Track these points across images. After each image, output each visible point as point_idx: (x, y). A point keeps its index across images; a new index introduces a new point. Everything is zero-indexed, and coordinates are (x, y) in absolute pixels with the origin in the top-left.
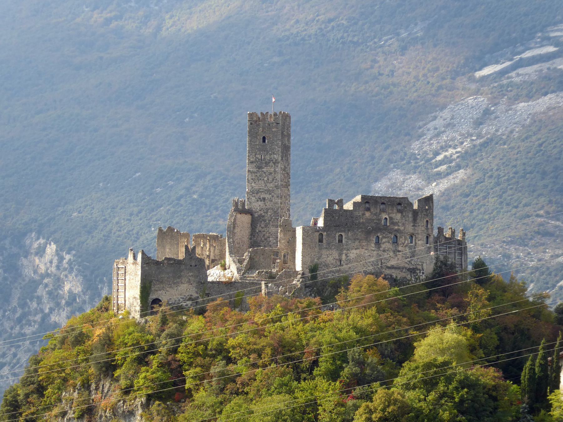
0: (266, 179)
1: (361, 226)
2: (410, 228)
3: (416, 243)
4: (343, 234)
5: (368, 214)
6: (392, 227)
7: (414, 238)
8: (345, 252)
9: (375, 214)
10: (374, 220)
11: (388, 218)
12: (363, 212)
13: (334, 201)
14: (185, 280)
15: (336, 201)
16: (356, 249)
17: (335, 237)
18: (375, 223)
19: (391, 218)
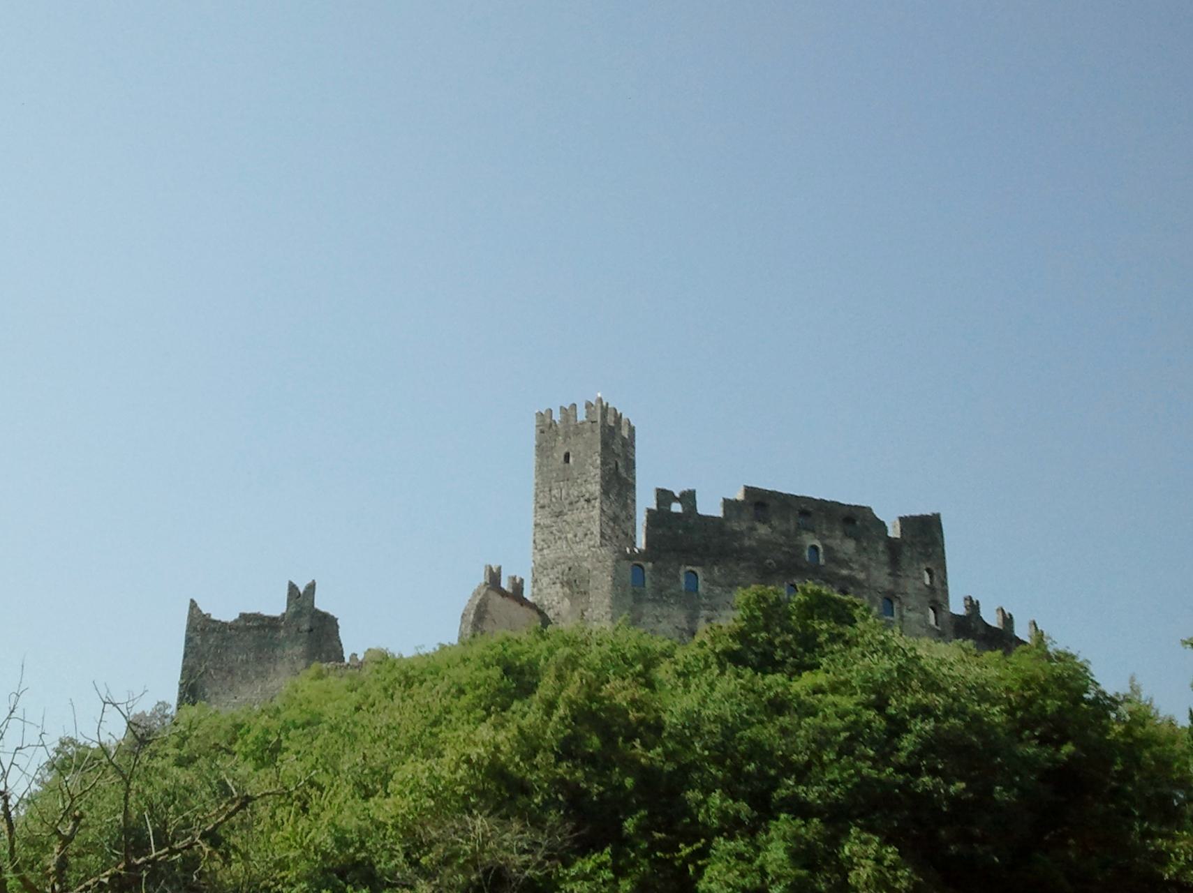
0: (570, 536)
2: (882, 577)
4: (698, 570)
5: (763, 530)
6: (832, 567)
7: (896, 605)
8: (704, 612)
11: (820, 546)
13: (672, 493)
17: (676, 578)
18: (784, 553)
19: (828, 549)
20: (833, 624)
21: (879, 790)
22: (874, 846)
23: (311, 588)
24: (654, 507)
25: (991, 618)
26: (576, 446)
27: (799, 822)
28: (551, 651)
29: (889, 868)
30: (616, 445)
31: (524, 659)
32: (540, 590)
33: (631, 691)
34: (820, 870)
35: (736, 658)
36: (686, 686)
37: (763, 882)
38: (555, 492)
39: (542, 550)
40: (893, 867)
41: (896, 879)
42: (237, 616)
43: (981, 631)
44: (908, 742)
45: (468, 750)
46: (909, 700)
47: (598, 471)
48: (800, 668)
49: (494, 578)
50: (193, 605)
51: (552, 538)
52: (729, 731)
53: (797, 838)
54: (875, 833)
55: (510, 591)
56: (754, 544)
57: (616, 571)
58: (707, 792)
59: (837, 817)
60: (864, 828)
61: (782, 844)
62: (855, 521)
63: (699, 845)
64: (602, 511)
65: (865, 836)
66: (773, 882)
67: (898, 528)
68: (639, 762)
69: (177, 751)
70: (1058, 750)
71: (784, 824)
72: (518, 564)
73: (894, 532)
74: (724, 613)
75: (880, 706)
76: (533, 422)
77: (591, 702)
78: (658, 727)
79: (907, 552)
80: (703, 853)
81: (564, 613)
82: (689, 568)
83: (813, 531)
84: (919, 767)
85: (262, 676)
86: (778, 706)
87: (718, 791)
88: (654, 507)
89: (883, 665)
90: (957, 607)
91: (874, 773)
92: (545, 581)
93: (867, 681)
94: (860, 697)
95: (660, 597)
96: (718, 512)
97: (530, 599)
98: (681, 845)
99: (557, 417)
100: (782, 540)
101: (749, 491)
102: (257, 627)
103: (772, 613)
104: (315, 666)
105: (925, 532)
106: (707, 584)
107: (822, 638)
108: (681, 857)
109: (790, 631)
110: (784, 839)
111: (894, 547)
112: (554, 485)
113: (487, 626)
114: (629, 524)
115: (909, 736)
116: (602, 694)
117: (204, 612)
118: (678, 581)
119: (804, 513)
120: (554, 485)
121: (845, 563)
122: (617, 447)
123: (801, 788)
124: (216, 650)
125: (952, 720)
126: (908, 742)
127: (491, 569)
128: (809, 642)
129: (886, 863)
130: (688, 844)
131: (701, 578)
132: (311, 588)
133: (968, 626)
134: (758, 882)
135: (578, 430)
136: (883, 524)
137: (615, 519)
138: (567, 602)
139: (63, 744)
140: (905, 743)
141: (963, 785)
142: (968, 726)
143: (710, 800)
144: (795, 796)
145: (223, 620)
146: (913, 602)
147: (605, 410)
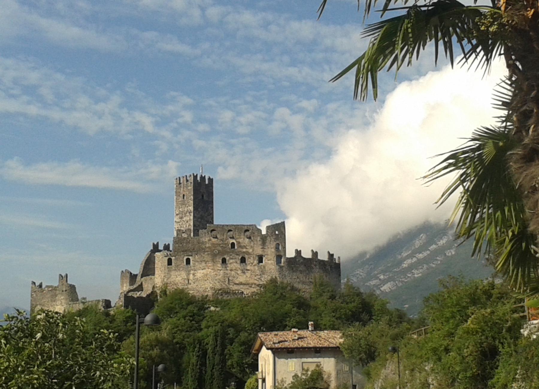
8: (192, 272)
12: (208, 238)
14: (58, 303)
17: (183, 261)
74: (199, 271)
118: (184, 262)
121: (245, 247)
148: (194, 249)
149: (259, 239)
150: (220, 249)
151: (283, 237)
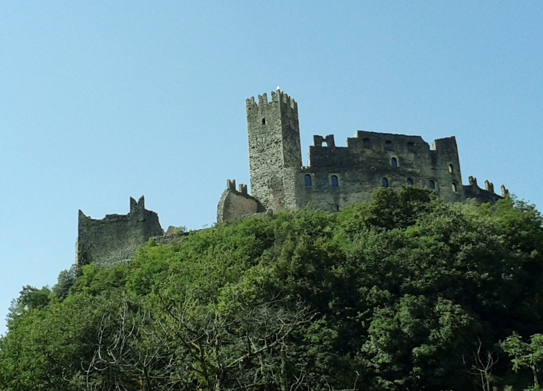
0: (268, 161)
1: (361, 165)
2: (428, 171)
3: (439, 189)
4: (337, 175)
5: (368, 152)
8: (342, 195)
9: (379, 153)
10: (377, 159)
12: (361, 150)
13: (322, 137)
14: (132, 240)
15: (324, 138)
16: (357, 192)
17: (327, 179)
19: (401, 159)
20: (419, 202)
21: (450, 280)
22: (450, 305)
23: (142, 199)
24: (313, 145)
25: (483, 186)
26: (269, 116)
27: (414, 297)
28: (279, 225)
29: (457, 314)
30: (288, 112)
31: (266, 229)
32: (255, 190)
33: (328, 243)
34: (426, 318)
35: (373, 222)
36: (351, 237)
37: (399, 326)
38: (259, 140)
39: (254, 170)
40: (459, 314)
41: (461, 320)
42: (105, 217)
43: (478, 193)
44: (460, 256)
45: (254, 278)
46: (459, 236)
47: (281, 127)
48: (405, 225)
49: (232, 186)
50: (80, 212)
51: (259, 163)
52: (378, 259)
53: (413, 304)
54: (449, 300)
55: (241, 191)
56: (364, 159)
57: (297, 179)
58: (370, 287)
59: (430, 293)
60: (444, 297)
61: (407, 308)
62: (414, 143)
63: (367, 312)
64: (284, 147)
65: (445, 301)
66: (403, 326)
67: (435, 145)
68: (334, 276)
69: (87, 288)
70: (530, 254)
71: (407, 299)
72: (243, 178)
73: (433, 148)
74: (352, 195)
75: (446, 240)
76: (245, 104)
77: (310, 250)
78: (344, 258)
79: (440, 158)
80: (370, 315)
81: (270, 201)
82: (333, 174)
83: (393, 151)
84: (466, 267)
85: (120, 245)
86: (399, 244)
87: (375, 286)
88: (313, 145)
89: (445, 220)
90: (466, 182)
91: (447, 272)
92: (258, 185)
93: (439, 229)
94: (436, 236)
95: (320, 189)
96: (346, 145)
97: (251, 195)
98: (358, 312)
99: (257, 101)
100: (378, 156)
101: (360, 133)
102: (114, 220)
103: (388, 200)
104: (151, 239)
105: (448, 146)
106: (342, 182)
107: (415, 209)
108: (358, 318)
109: (399, 207)
110: (408, 306)
111: (433, 155)
112: (258, 136)
113: (231, 211)
114: (297, 153)
115: (461, 253)
116: (314, 245)
117: (87, 216)
118: (328, 181)
119: (388, 142)
120: (258, 136)
122: (289, 115)
123: (413, 282)
124: (94, 234)
125: (481, 244)
126: (460, 256)
127: (230, 182)
128: (409, 212)
129: (456, 312)
130: (361, 312)
131: (339, 179)
132: (142, 199)
133: (472, 190)
134: (397, 326)
135: (269, 106)
136: (427, 143)
137: (291, 151)
138: (272, 196)
139: (24, 289)
140: (458, 256)
141: (487, 274)
142: (488, 245)
143: (371, 292)
144: (411, 285)
145: (97, 219)
146: (444, 182)
147: (282, 95)
148: (341, 164)
149: (427, 156)
150: (377, 164)
151: (456, 157)
